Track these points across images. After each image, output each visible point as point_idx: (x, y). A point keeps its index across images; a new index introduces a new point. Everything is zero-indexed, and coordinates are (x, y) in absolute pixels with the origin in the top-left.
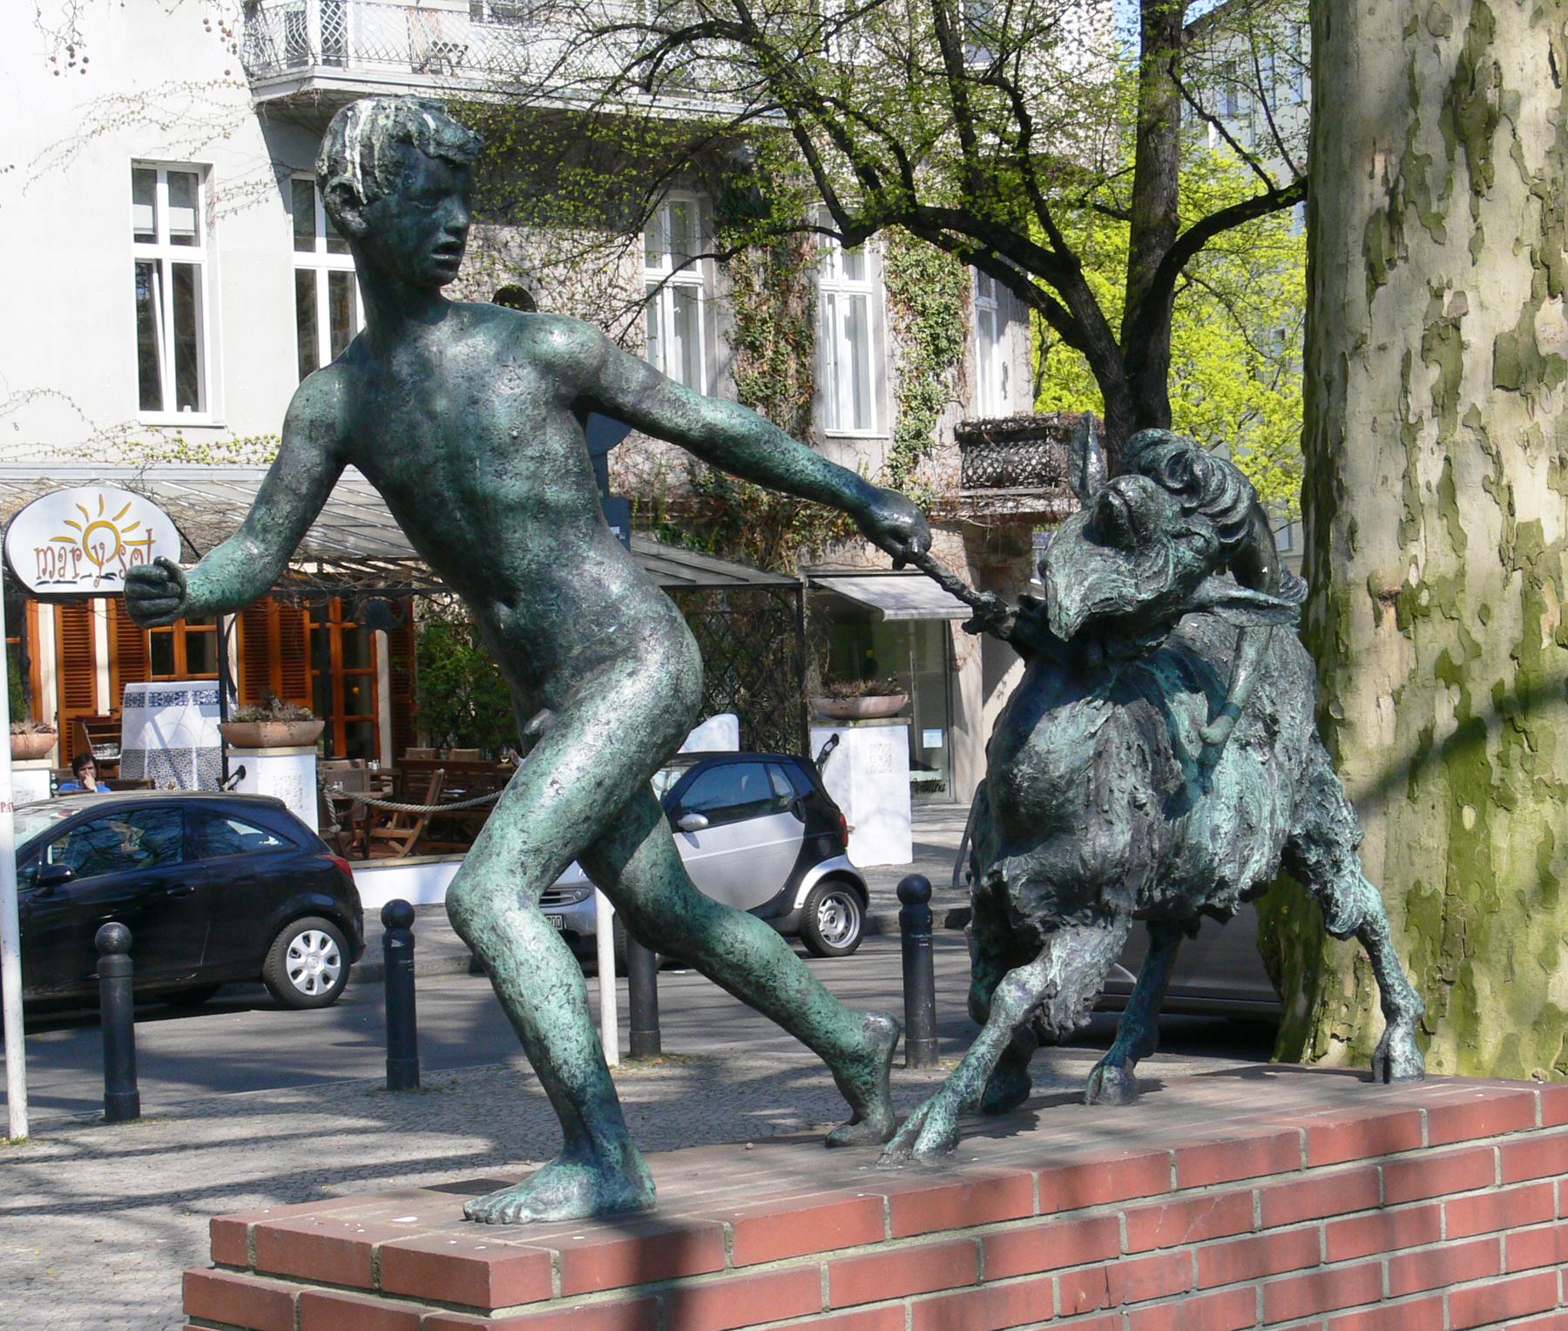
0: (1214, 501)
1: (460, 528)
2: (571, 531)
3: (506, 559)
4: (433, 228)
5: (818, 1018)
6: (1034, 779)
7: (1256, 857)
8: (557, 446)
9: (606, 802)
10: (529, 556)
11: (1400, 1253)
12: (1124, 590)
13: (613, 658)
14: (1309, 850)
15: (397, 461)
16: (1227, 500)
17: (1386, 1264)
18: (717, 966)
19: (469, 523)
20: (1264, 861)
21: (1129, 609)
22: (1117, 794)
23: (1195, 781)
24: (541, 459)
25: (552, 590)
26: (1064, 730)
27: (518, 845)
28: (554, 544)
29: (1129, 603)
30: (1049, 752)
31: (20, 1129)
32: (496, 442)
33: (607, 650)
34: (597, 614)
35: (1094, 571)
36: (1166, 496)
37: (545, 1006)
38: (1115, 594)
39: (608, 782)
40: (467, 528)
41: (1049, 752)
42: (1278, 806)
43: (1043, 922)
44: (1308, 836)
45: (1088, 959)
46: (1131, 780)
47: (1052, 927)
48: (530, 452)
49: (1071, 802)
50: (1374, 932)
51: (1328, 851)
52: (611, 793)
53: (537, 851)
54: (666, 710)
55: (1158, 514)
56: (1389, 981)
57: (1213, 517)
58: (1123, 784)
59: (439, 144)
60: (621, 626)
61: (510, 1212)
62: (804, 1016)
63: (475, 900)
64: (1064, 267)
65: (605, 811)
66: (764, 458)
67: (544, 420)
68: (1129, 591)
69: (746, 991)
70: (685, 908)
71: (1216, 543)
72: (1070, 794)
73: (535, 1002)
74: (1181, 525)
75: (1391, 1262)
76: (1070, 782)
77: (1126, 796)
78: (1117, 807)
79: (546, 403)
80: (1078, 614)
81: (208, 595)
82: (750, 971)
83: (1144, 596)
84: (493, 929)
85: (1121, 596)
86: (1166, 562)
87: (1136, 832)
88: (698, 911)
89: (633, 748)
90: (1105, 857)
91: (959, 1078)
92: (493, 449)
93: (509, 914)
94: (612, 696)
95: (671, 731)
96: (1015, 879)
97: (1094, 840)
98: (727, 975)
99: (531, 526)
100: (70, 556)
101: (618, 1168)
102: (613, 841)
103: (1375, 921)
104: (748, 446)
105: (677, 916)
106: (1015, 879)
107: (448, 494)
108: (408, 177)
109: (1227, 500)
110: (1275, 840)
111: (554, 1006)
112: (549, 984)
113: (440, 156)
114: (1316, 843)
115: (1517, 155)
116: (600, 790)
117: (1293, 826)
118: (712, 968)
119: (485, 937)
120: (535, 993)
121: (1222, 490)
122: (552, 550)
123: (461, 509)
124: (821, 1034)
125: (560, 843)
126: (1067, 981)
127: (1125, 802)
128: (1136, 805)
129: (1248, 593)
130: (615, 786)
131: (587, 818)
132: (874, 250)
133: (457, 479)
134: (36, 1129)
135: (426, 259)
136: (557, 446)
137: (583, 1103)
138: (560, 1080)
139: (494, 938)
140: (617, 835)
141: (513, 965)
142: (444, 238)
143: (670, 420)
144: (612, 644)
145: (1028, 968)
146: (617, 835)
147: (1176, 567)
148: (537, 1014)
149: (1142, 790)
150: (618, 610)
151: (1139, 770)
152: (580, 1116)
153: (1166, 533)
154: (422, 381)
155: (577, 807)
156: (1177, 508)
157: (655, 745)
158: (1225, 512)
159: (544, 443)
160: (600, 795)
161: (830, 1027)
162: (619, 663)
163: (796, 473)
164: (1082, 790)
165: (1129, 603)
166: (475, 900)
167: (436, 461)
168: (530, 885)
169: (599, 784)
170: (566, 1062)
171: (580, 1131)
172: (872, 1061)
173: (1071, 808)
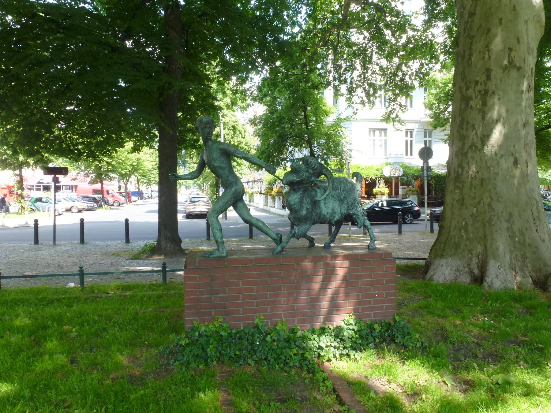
46: (306, 205)
128: (307, 208)
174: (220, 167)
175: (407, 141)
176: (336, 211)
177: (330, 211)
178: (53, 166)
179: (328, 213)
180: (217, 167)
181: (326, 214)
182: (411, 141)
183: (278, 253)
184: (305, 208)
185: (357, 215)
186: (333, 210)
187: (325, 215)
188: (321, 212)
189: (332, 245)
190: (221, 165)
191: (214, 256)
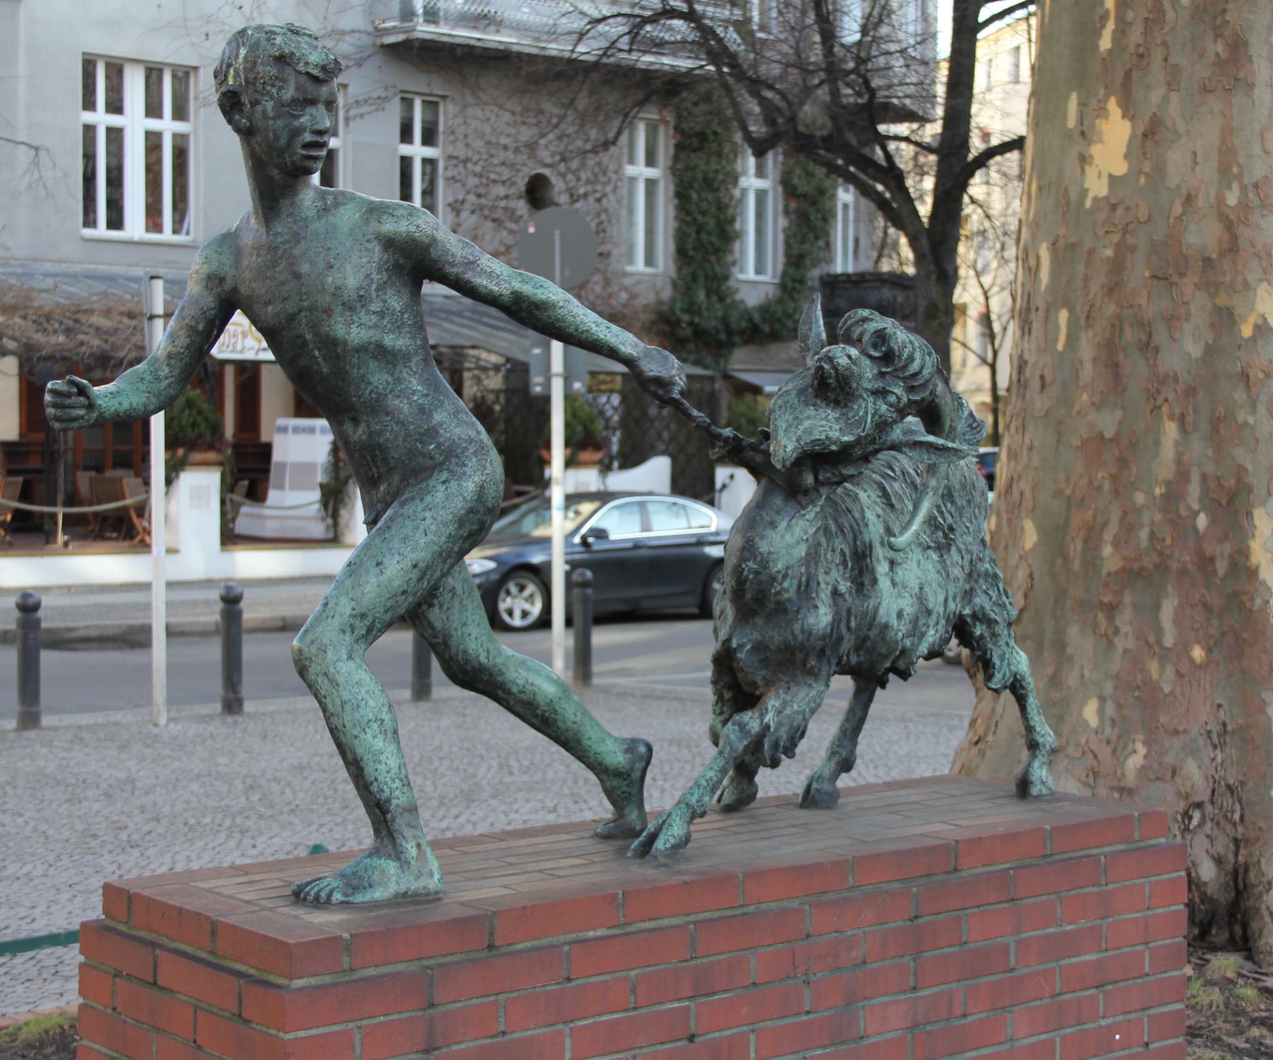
0: (905, 367)
1: (318, 363)
2: (404, 370)
3: (352, 390)
4: (296, 132)
5: (589, 743)
6: (757, 573)
7: (932, 632)
8: (395, 304)
9: (420, 579)
10: (370, 388)
11: (1024, 935)
12: (831, 434)
13: (433, 469)
14: (975, 625)
15: (270, 308)
16: (915, 367)
17: (1013, 945)
18: (512, 702)
19: (325, 360)
20: (938, 635)
21: (834, 448)
22: (823, 586)
23: (887, 574)
24: (382, 314)
25: (387, 414)
26: (783, 536)
27: (348, 611)
28: (390, 379)
29: (834, 443)
30: (770, 553)
31: (163, 721)
32: (346, 298)
33: (429, 463)
34: (422, 435)
35: (809, 418)
36: (868, 362)
37: (362, 736)
38: (823, 437)
39: (421, 565)
40: (323, 364)
41: (770, 553)
42: (951, 594)
43: (764, 678)
44: (974, 616)
45: (796, 707)
46: (835, 575)
47: (769, 684)
48: (373, 308)
49: (787, 591)
50: (1023, 688)
51: (989, 626)
52: (424, 573)
53: (363, 616)
54: (471, 511)
55: (861, 377)
56: (1032, 723)
57: (904, 379)
58: (828, 578)
59: (307, 64)
60: (439, 446)
61: (323, 894)
62: (579, 742)
63: (313, 650)
64: (893, 176)
65: (420, 586)
66: (558, 320)
67: (385, 283)
68: (834, 434)
69: (534, 721)
70: (488, 658)
71: (905, 399)
72: (786, 585)
73: (355, 732)
74: (878, 385)
75: (1019, 943)
76: (785, 576)
77: (830, 588)
78: (823, 596)
79: (387, 270)
80: (793, 451)
81: (117, 406)
82: (537, 707)
83: (846, 439)
84: (325, 674)
85: (827, 438)
86: (866, 413)
87: (837, 614)
88: (498, 660)
89: (443, 539)
90: (810, 633)
91: (692, 794)
92: (343, 304)
93: (339, 664)
94: (428, 499)
95: (475, 527)
96: (741, 646)
97: (803, 619)
98: (518, 708)
99: (373, 365)
100: (240, 336)
101: (413, 862)
102: (431, 605)
103: (1023, 678)
104: (546, 310)
105: (480, 664)
106: (741, 646)
107: (309, 337)
108: (281, 88)
109: (915, 367)
110: (948, 620)
111: (369, 736)
112: (366, 719)
113: (307, 73)
114: (980, 620)
115: (702, 67)
116: (415, 571)
117: (963, 607)
118: (508, 703)
119: (319, 680)
120: (355, 725)
121: (911, 359)
122: (388, 383)
123: (319, 349)
124: (591, 755)
125: (382, 610)
126: (779, 724)
127: (828, 592)
128: (835, 593)
129: (931, 438)
130: (428, 567)
131: (404, 592)
132: (773, 160)
133: (314, 326)
134: (170, 720)
135: (294, 153)
136: (395, 304)
137: (388, 811)
138: (371, 793)
139: (326, 681)
140: (435, 601)
141: (338, 702)
142: (308, 137)
143: (486, 287)
144: (432, 458)
145: (749, 713)
146: (435, 601)
147: (873, 416)
148: (356, 742)
149: (842, 582)
150: (437, 433)
151: (841, 568)
152: (386, 821)
153: (866, 390)
154: (291, 248)
155: (396, 583)
156: (875, 371)
157: (461, 537)
158: (915, 375)
159: (385, 301)
160: (415, 575)
161: (598, 750)
162: (435, 475)
163: (583, 332)
164: (795, 582)
165: (834, 443)
166: (313, 650)
167: (300, 311)
168: (357, 641)
169: (415, 566)
170: (376, 780)
171: (384, 833)
172: (629, 776)
173: (786, 596)
174: (382, 354)
175: (89, 130)
176: (931, 606)
177: (908, 605)
178: (929, 200)
179: (900, 615)
180: (362, 349)
181: (894, 621)
182: (89, 104)
183: (1226, 575)
184: (825, 594)
185: (991, 623)
186: (921, 598)
187: (886, 627)
188: (876, 610)
189: (844, 781)
190: (389, 340)
191: (378, 894)
